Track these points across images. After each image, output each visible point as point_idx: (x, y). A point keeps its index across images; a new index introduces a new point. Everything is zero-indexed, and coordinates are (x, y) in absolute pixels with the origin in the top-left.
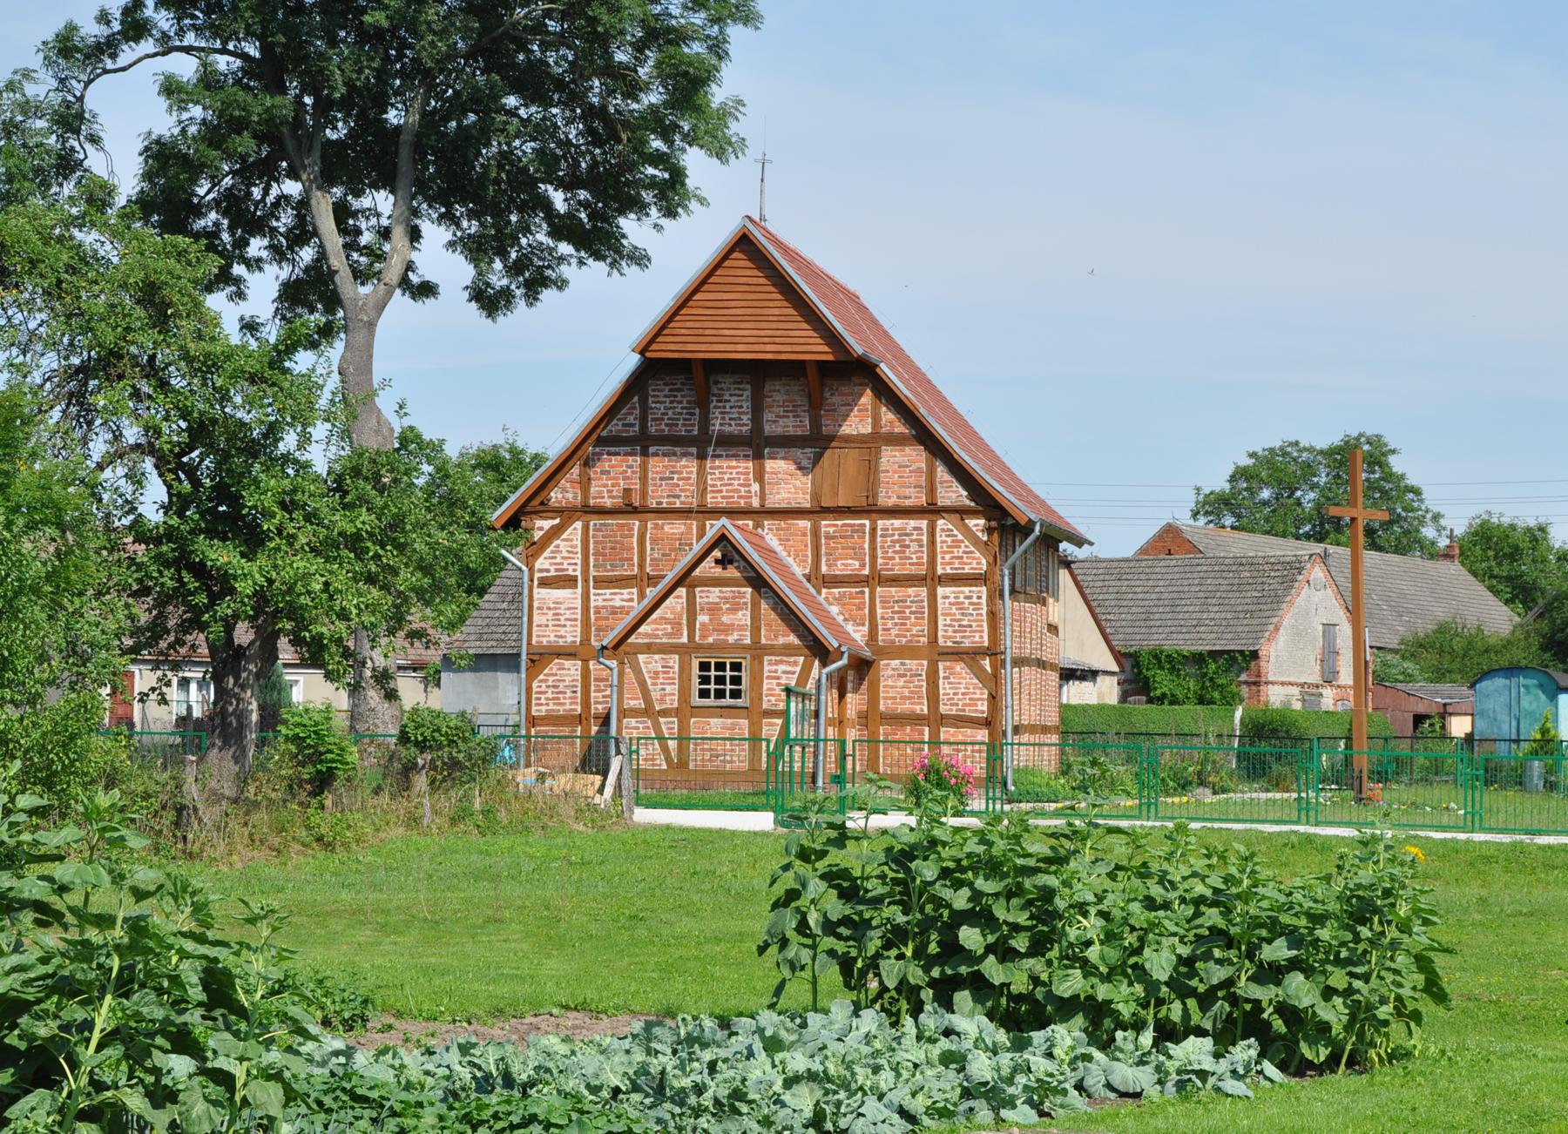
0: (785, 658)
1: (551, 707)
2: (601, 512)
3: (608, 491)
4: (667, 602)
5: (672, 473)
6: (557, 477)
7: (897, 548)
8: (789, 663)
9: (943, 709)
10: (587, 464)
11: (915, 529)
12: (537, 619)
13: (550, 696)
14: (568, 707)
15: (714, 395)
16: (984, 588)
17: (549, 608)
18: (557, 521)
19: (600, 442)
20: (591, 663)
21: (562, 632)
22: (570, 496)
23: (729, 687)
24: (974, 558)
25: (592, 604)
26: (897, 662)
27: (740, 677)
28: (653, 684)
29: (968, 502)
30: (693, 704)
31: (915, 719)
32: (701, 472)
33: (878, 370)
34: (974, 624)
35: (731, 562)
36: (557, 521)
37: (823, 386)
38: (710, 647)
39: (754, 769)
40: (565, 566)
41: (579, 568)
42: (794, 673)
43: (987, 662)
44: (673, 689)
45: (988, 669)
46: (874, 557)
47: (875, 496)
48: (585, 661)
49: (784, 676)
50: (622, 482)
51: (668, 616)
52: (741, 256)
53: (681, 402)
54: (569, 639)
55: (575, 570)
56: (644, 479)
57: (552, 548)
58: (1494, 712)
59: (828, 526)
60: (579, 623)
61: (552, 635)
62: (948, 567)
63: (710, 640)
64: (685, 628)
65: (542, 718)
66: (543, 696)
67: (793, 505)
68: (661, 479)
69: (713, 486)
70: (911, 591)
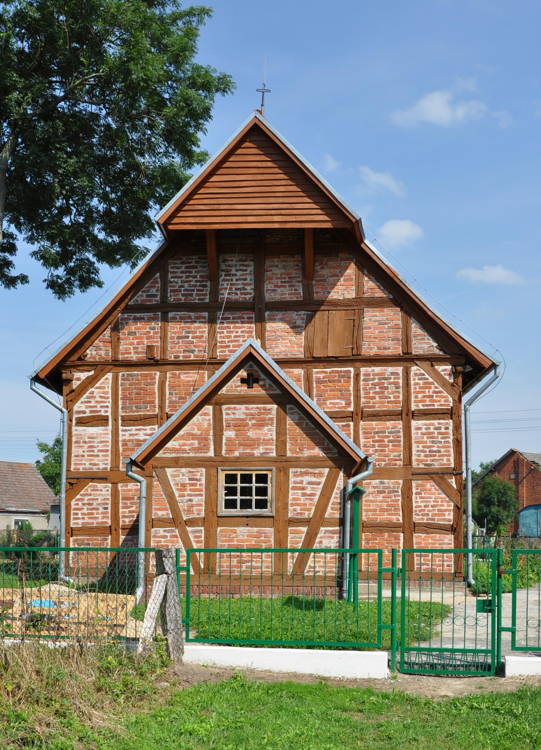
0: (310, 470)
1: (87, 520)
2: (128, 365)
3: (134, 348)
4: (195, 419)
5: (188, 332)
6: (93, 338)
7: (378, 389)
8: (314, 475)
9: (416, 518)
10: (116, 329)
11: (392, 374)
12: (75, 450)
13: (85, 511)
14: (100, 520)
15: (223, 270)
16: (451, 421)
17: (85, 442)
18: (92, 373)
19: (128, 309)
20: (120, 485)
21: (96, 460)
22: (102, 353)
23: (254, 498)
24: (443, 397)
25: (121, 438)
26: (377, 481)
27: (266, 489)
28: (181, 496)
29: (437, 351)
30: (220, 514)
31: (391, 527)
32: (212, 334)
33: (363, 246)
34: (442, 450)
35: (257, 381)
36: (92, 373)
37: (315, 261)
38: (237, 460)
39: (280, 573)
40: (98, 409)
41: (109, 410)
42: (319, 484)
43: (453, 480)
44: (200, 500)
45: (455, 486)
46: (357, 397)
47: (359, 347)
48: (115, 484)
49: (309, 486)
50: (146, 341)
51: (196, 431)
52: (251, 145)
53: (195, 277)
54: (102, 466)
55: (106, 412)
56: (164, 338)
57: (87, 394)
58: (529, 524)
59: (318, 373)
60: (109, 453)
61: (87, 463)
62: (420, 405)
63: (237, 454)
64: (212, 443)
65: (79, 529)
66: (80, 512)
67: (289, 356)
68: (179, 338)
69: (222, 342)
70: (389, 424)
